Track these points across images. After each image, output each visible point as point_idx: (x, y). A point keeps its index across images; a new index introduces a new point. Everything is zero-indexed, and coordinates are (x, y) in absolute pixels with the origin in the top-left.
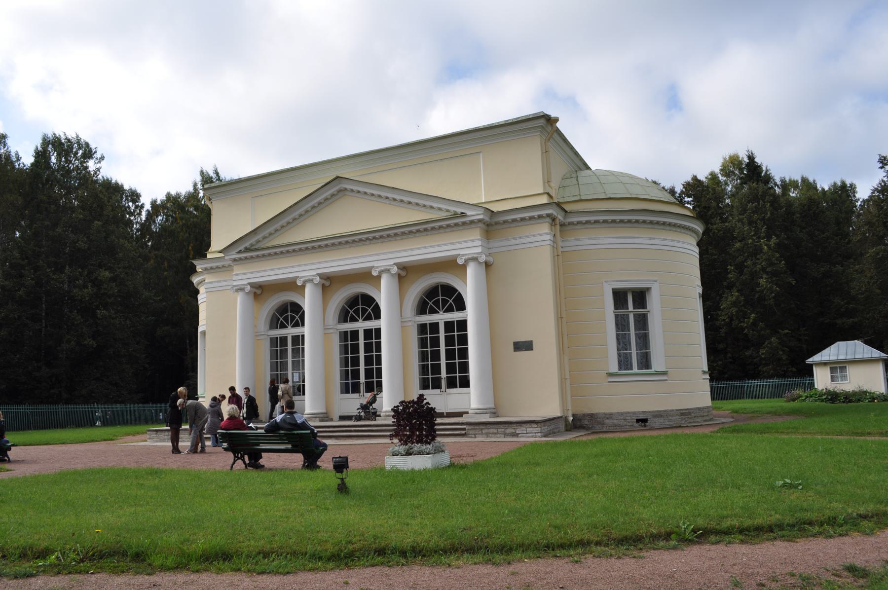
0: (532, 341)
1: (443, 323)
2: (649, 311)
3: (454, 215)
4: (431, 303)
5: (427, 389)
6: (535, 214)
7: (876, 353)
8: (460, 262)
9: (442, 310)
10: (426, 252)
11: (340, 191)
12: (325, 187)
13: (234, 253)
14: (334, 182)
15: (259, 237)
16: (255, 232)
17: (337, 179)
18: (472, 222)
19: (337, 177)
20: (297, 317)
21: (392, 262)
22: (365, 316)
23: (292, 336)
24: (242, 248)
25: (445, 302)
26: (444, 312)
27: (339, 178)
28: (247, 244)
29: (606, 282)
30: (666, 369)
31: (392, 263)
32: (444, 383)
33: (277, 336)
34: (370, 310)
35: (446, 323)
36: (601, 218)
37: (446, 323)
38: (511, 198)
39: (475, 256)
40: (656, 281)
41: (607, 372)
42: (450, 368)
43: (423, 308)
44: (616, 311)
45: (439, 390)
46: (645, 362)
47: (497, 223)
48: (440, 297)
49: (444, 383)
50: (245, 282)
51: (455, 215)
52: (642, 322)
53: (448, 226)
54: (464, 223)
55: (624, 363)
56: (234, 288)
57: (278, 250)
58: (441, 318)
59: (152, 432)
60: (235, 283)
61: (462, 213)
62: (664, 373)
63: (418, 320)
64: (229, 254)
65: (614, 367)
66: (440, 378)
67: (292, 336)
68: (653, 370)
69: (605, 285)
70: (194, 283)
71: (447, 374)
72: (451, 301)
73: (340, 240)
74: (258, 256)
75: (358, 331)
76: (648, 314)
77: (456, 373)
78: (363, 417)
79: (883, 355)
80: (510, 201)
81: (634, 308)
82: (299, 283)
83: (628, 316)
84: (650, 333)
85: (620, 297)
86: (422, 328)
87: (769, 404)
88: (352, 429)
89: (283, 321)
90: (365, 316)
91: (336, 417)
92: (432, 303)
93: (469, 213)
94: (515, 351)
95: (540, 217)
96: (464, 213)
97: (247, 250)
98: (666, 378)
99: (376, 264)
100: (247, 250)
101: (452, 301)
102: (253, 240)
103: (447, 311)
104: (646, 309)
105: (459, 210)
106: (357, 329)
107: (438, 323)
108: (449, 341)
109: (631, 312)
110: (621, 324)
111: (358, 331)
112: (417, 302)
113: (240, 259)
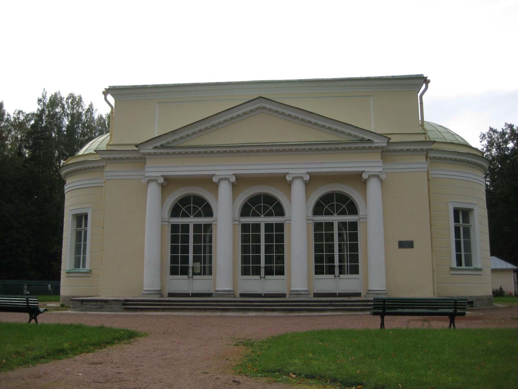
0: (413, 241)
1: (193, 226)
2: (471, 225)
3: (361, 140)
4: (254, 208)
5: (322, 274)
6: (419, 147)
7: (510, 266)
8: (215, 180)
9: (336, 213)
10: (357, 166)
11: (259, 108)
12: (247, 103)
13: (151, 147)
14: (256, 100)
15: (177, 137)
16: (174, 132)
17: (259, 99)
18: (377, 148)
19: (261, 97)
20: (200, 209)
21: (231, 173)
22: (195, 214)
23: (194, 225)
24: (158, 144)
25: (195, 209)
26: (338, 214)
27: (261, 98)
28: (164, 142)
29: (450, 202)
30: (482, 267)
31: (231, 174)
32: (263, 271)
33: (250, 223)
34: (271, 208)
35: (195, 226)
36: (449, 156)
37: (195, 226)
38: (397, 134)
39: (378, 174)
40: (90, 208)
41: (450, 267)
42: (268, 260)
43: (175, 212)
44: (86, 230)
45: (259, 276)
46: (469, 263)
47: (389, 151)
48: (192, 205)
49: (263, 271)
50: (159, 174)
51: (363, 140)
52: (467, 232)
53: (350, 148)
54: (370, 148)
55: (459, 263)
56: (146, 178)
57: (190, 150)
58: (192, 221)
59: (76, 302)
60: (147, 174)
61: (369, 140)
62: (480, 270)
63: (315, 219)
64: (147, 148)
65: (454, 264)
66: (260, 268)
67: (194, 225)
68: (473, 267)
69: (450, 204)
70: (62, 174)
71: (265, 264)
72: (326, 207)
73: (193, 150)
74: (167, 154)
75: (260, 224)
76: (470, 227)
77: (252, 266)
78: (263, 295)
79: (515, 267)
80: (397, 135)
81: (463, 223)
82: (288, 178)
83: (82, 231)
84: (471, 241)
85: (456, 212)
86: (175, 228)
87: (253, 303)
88: (220, 303)
89: (201, 210)
90: (195, 214)
91: (166, 294)
92: (255, 208)
93: (375, 140)
94: (399, 248)
95: (422, 150)
96: (372, 140)
97: (162, 147)
98: (481, 273)
99: (366, 169)
100: (162, 147)
101: (254, 207)
102: (170, 139)
103: (197, 216)
104: (469, 223)
105: (367, 137)
106: (249, 223)
107: (189, 225)
108: (268, 238)
109: (461, 225)
110: (457, 230)
111: (260, 224)
112: (173, 206)
113: (155, 154)
